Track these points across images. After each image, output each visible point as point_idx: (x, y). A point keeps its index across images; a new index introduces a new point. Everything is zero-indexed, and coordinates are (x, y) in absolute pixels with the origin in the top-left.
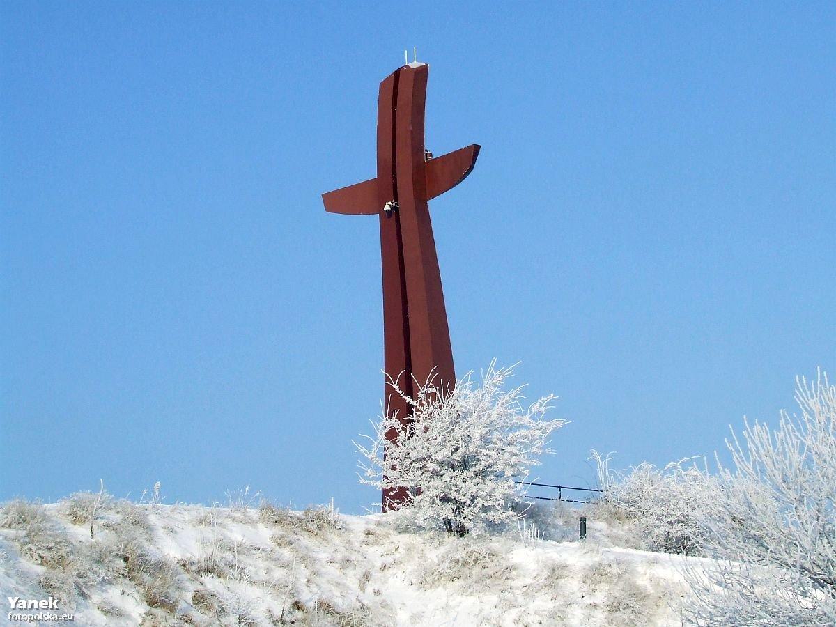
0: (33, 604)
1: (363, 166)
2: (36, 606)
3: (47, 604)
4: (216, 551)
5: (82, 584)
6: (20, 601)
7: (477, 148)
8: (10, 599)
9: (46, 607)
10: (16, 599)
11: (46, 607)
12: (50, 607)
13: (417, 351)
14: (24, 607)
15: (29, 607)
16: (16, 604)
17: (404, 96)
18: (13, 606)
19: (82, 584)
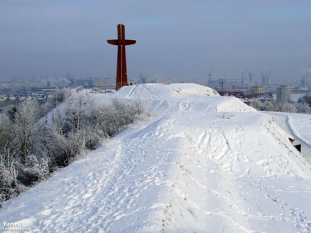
0: (12, 224)
1: (128, 48)
2: (13, 225)
3: (17, 224)
4: (61, 223)
5: (96, 159)
6: (7, 223)
7: (289, 138)
8: (4, 222)
9: (17, 226)
10: (6, 222)
11: (17, 226)
12: (19, 225)
13: (121, 42)
14: (9, 225)
15: (11, 225)
16: (6, 225)
17: (121, 29)
18: (5, 225)
19: (96, 159)
